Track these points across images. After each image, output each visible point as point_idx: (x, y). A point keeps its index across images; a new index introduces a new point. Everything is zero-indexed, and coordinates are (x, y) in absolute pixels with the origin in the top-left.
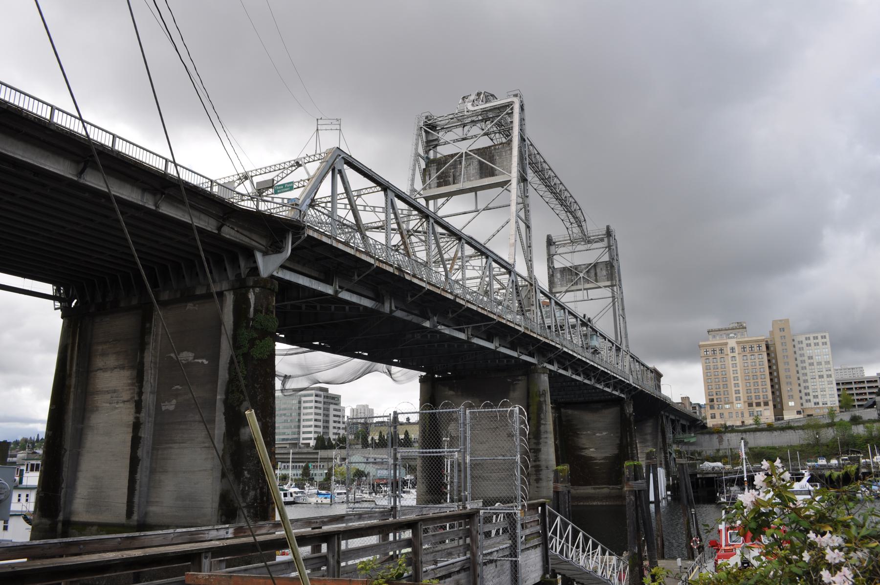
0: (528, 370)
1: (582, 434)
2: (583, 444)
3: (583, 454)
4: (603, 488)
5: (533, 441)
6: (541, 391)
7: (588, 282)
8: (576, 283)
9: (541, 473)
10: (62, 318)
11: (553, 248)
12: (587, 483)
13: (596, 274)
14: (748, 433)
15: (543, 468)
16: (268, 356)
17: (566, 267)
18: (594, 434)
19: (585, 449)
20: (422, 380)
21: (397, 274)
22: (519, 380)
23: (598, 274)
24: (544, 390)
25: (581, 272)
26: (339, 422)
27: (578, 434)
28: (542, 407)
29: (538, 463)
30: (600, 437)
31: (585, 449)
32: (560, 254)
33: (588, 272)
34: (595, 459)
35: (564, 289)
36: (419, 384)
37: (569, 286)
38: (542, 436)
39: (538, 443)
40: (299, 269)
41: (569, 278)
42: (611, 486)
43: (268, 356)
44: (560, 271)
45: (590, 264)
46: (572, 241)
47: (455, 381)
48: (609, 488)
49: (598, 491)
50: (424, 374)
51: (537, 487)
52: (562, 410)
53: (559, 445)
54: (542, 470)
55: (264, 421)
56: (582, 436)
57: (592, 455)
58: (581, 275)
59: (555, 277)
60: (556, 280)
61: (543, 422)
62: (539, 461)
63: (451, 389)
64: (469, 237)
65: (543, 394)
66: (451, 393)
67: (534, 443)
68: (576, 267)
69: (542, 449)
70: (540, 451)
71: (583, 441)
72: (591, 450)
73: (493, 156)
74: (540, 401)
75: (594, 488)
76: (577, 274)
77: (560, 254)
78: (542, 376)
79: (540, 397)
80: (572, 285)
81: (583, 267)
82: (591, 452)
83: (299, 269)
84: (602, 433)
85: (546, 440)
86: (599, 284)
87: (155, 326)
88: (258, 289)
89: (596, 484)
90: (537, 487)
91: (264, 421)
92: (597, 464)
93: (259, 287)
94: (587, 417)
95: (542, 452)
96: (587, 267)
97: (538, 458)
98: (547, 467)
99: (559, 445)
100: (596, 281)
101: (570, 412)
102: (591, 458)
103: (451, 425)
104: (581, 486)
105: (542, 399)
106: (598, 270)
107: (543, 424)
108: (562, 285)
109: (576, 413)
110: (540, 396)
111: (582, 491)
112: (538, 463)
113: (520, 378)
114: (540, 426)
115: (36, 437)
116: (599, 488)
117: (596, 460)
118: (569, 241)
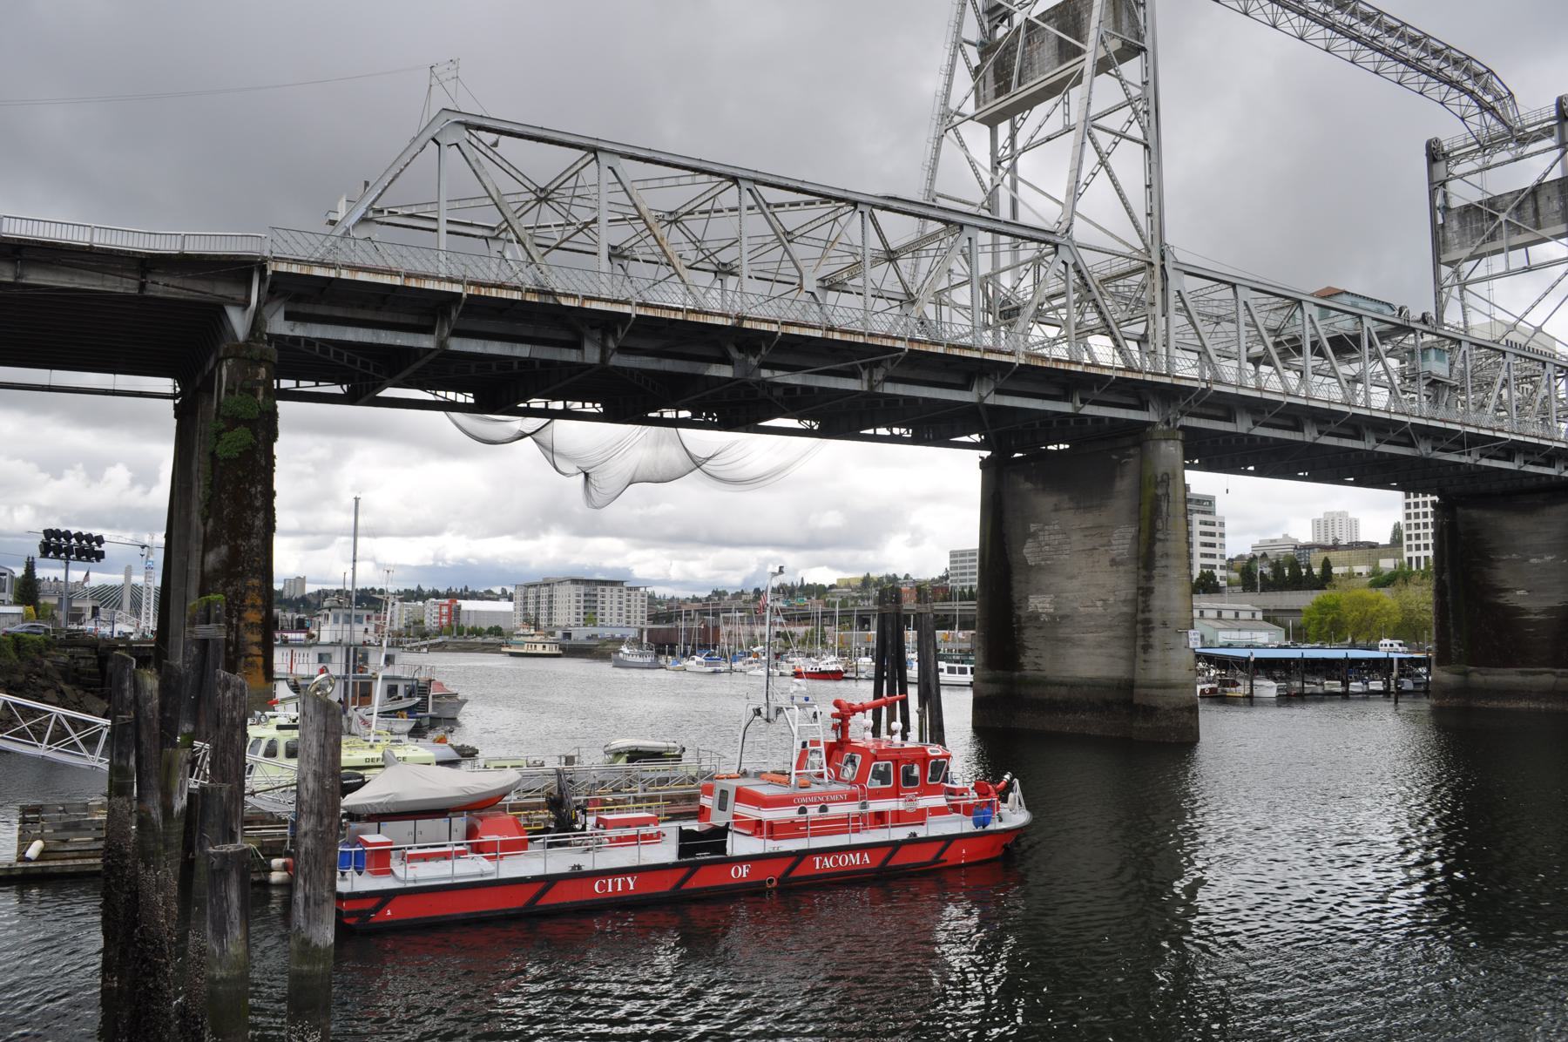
0: (1137, 433)
1: (1499, 561)
2: (1502, 581)
3: (1501, 601)
4: (1541, 673)
5: (1143, 572)
6: (1159, 475)
7: (1518, 230)
8: (1492, 237)
9: (1152, 633)
10: (175, 417)
11: (1440, 168)
12: (1508, 662)
13: (1536, 211)
14: (1158, 548)
15: (1156, 624)
16: (240, 453)
17: (1471, 205)
18: (1526, 560)
19: (1507, 590)
20: (984, 464)
21: (537, 300)
22: (1130, 456)
23: (1542, 211)
24: (1167, 474)
25: (1504, 211)
26: (1213, 556)
27: (1492, 560)
28: (1160, 506)
29: (1147, 615)
30: (1537, 565)
31: (1507, 590)
32: (1461, 177)
33: (1518, 208)
34: (1525, 611)
35: (1466, 253)
36: (980, 472)
37: (1478, 243)
38: (1158, 564)
39: (1149, 578)
40: (338, 312)
41: (1477, 228)
42: (1560, 671)
43: (240, 453)
44: (1459, 214)
45: (1524, 190)
46: (1482, 146)
47: (1033, 464)
48: (1554, 673)
49: (1530, 678)
50: (986, 454)
51: (1145, 661)
52: (1460, 510)
53: (1448, 583)
54: (1153, 628)
55: (233, 543)
56: (1500, 564)
57: (1519, 605)
58: (1503, 217)
59: (1447, 230)
60: (1449, 235)
61: (1159, 536)
62: (1150, 611)
63: (1028, 479)
64: (884, 197)
65: (1163, 481)
66: (1029, 485)
67: (1145, 577)
68: (1492, 202)
69: (1156, 589)
70: (1152, 592)
71: (1503, 574)
72: (1518, 593)
73: (1079, 14)
74: (1156, 495)
75: (1523, 673)
76: (1493, 217)
77: (1461, 177)
78: (1163, 445)
79: (1156, 488)
80: (1483, 242)
81: (1508, 198)
82: (1519, 597)
83: (338, 312)
84: (1542, 558)
85: (1164, 571)
86: (1542, 233)
87: (202, 421)
88: (231, 360)
89: (1524, 664)
90: (1145, 661)
91: (233, 543)
92: (1529, 623)
93: (231, 357)
94: (1513, 524)
95: (1156, 592)
96: (1517, 198)
97: (1148, 606)
98: (1164, 624)
99: (1448, 583)
100: (1538, 226)
101: (1475, 513)
102: (1519, 611)
103: (1028, 545)
104: (1497, 666)
105: (1160, 492)
106: (1542, 201)
107: (1160, 540)
108: (1462, 246)
109: (1488, 515)
110: (1157, 485)
111: (1496, 678)
112: (1147, 615)
113: (1132, 451)
114: (1155, 544)
115: (799, 584)
116: (1534, 674)
117: (1531, 613)
118: (1477, 146)
